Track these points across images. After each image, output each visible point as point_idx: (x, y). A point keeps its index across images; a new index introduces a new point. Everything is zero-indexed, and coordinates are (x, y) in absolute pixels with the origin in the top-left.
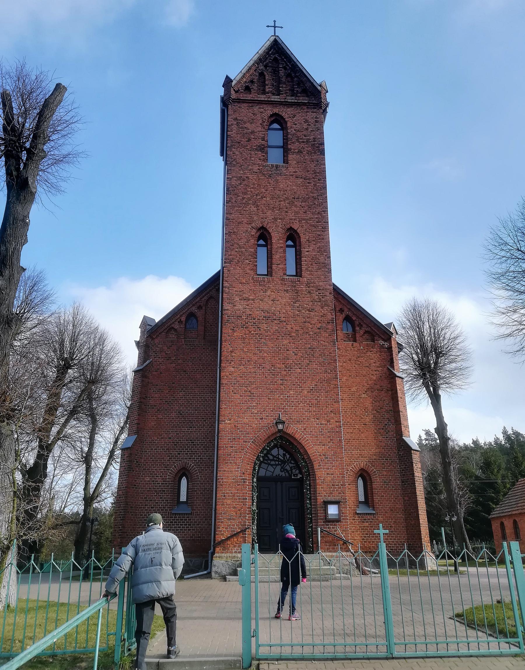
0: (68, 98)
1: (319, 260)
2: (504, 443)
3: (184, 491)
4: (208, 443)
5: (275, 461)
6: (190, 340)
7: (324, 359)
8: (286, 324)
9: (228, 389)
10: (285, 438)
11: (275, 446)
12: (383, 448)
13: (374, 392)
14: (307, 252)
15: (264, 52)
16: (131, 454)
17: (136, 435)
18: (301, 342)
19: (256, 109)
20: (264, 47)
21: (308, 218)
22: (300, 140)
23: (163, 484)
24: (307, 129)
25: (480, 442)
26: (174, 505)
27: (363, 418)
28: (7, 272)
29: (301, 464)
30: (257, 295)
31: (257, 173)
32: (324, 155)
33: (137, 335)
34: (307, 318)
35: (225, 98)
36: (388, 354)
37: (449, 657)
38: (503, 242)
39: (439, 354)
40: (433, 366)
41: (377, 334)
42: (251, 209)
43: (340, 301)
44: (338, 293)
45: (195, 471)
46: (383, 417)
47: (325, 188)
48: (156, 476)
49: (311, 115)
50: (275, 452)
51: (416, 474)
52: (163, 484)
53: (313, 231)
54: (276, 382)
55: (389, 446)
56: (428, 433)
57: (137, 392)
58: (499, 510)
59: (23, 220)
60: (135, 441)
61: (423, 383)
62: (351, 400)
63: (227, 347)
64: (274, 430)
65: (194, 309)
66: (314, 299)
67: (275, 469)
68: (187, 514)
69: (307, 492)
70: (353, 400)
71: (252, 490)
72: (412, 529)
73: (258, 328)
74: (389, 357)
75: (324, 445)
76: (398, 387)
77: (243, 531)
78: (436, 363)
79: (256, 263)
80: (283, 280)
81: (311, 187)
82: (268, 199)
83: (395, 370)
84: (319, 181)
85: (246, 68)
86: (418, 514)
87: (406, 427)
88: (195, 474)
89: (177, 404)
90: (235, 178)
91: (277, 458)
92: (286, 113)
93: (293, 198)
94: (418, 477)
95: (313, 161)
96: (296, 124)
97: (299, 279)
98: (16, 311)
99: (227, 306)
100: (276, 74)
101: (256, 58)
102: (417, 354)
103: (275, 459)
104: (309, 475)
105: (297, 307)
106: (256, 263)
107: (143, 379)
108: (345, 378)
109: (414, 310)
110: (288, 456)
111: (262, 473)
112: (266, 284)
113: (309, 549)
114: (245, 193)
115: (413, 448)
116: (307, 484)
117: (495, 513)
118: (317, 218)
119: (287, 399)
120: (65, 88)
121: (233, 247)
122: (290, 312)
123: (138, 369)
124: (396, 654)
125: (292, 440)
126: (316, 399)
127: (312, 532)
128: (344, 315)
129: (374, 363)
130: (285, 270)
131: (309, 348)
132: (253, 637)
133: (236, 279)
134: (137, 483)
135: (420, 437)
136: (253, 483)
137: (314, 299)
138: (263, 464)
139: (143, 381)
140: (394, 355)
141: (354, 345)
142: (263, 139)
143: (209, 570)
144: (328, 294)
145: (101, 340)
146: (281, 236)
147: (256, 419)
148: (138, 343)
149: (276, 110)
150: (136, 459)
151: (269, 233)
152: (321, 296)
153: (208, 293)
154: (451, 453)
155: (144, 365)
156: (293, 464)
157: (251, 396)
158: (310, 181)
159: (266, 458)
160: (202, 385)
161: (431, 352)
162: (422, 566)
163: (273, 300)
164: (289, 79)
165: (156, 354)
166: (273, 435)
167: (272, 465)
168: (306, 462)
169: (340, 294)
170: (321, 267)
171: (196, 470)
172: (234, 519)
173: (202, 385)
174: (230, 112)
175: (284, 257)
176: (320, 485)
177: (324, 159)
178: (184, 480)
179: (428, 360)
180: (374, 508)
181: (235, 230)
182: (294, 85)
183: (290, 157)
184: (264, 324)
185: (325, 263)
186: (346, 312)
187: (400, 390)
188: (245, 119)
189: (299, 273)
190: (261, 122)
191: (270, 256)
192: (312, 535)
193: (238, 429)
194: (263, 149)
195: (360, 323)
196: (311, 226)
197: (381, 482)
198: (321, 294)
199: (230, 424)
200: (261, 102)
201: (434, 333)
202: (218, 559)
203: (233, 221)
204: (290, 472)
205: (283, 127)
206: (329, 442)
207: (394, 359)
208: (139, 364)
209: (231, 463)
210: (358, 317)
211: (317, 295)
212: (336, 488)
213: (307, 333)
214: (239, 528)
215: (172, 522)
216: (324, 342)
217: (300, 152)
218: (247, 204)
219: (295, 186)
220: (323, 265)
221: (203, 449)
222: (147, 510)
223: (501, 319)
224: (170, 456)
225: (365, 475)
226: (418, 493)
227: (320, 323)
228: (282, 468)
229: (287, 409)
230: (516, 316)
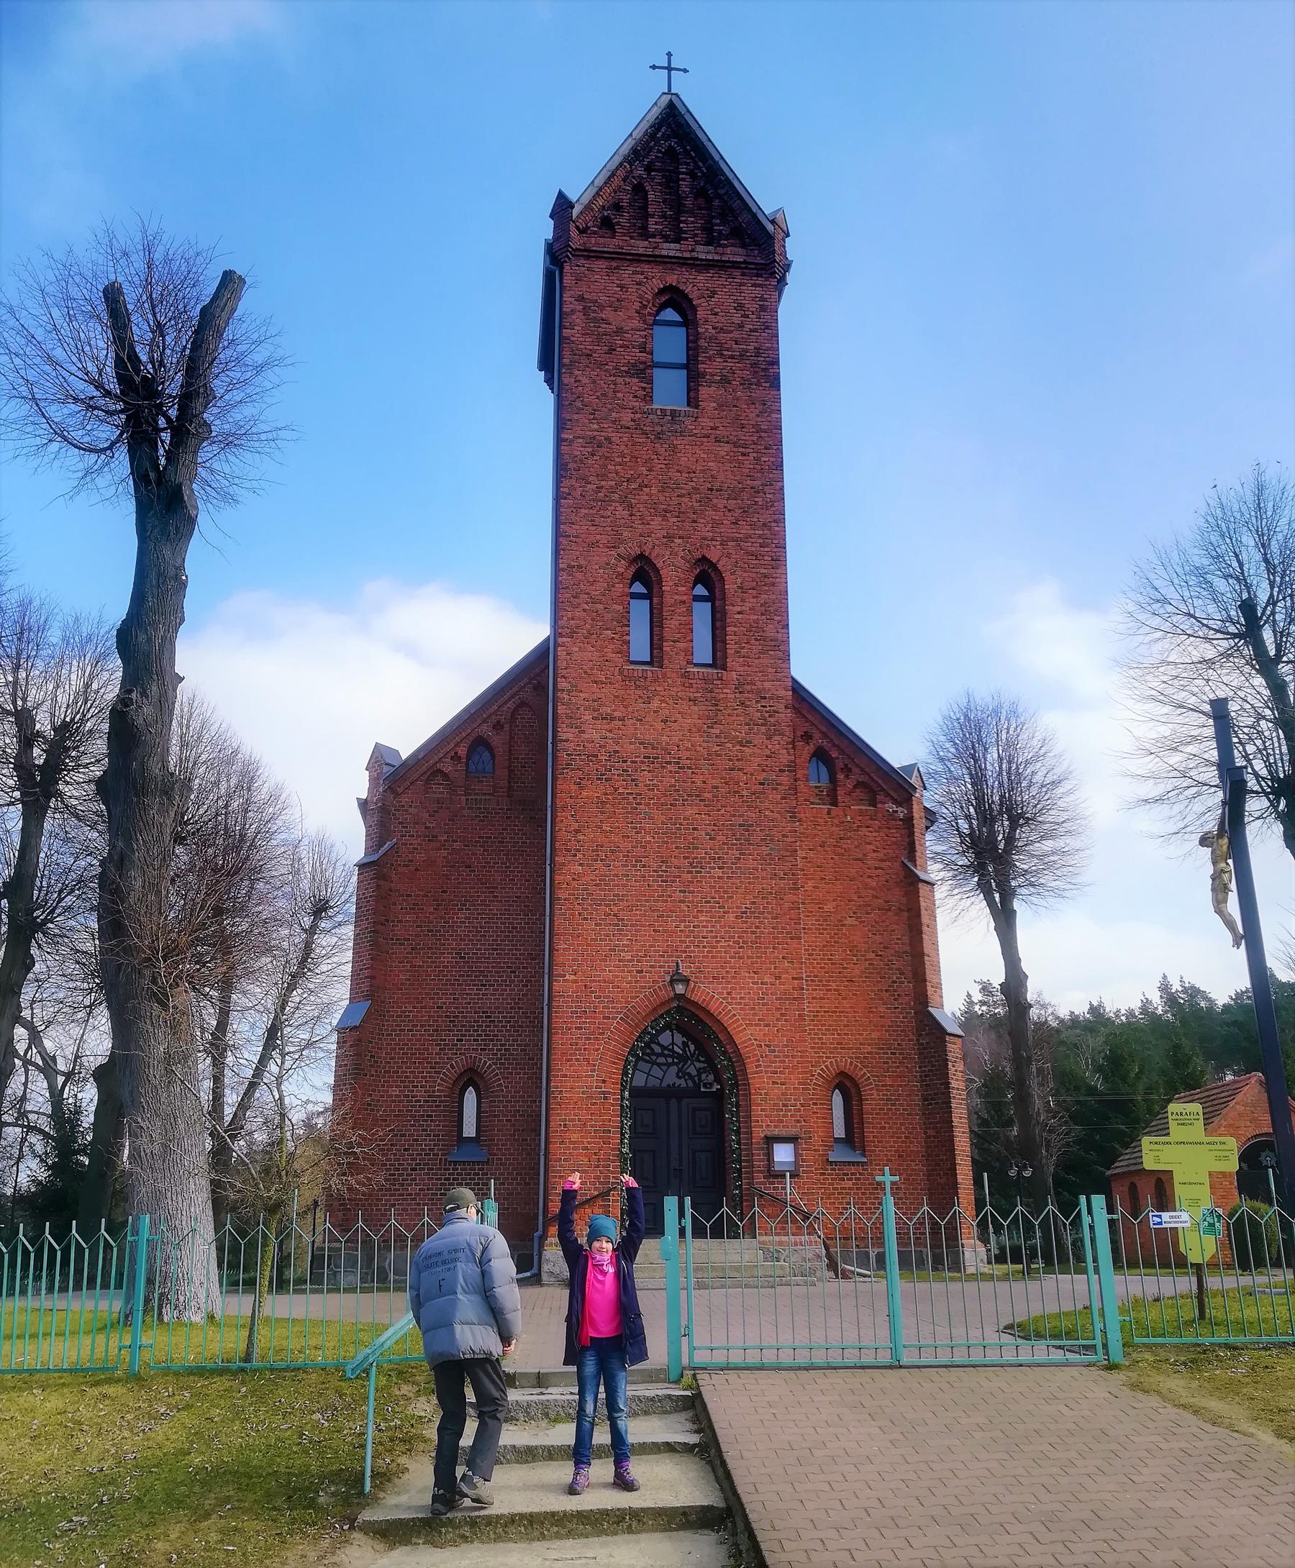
0: (248, 304)
1: (763, 631)
2: (1161, 1013)
3: (470, 1117)
4: (521, 1017)
5: (665, 1056)
6: (478, 798)
7: (771, 849)
8: (693, 773)
9: (569, 909)
10: (687, 1010)
11: (668, 1026)
12: (886, 1031)
13: (871, 913)
14: (739, 613)
15: (646, 133)
16: (360, 1040)
17: (368, 1000)
18: (723, 812)
19: (627, 273)
20: (643, 124)
21: (742, 536)
22: (726, 353)
23: (427, 1101)
24: (741, 326)
25: (1108, 1010)
26: (451, 1145)
27: (846, 968)
28: (154, 688)
29: (720, 1063)
30: (630, 709)
31: (629, 428)
32: (779, 390)
33: (361, 786)
34: (738, 760)
35: (556, 246)
36: (903, 832)
37: (985, 1366)
38: (1158, 596)
39: (1017, 818)
40: (1002, 846)
41: (883, 790)
42: (617, 513)
43: (805, 717)
44: (803, 701)
45: (494, 1076)
46: (888, 965)
47: (780, 466)
48: (413, 1086)
49: (751, 292)
50: (665, 1038)
51: (954, 1084)
52: (427, 1101)
53: (752, 566)
54: (670, 896)
55: (900, 1026)
56: (986, 988)
57: (368, 910)
58: (1129, 1159)
59: (177, 578)
60: (368, 1014)
61: (978, 884)
62: (823, 929)
63: (567, 822)
64: (665, 994)
67: (665, 1073)
68: (478, 1163)
69: (731, 1119)
70: (826, 929)
71: (621, 1115)
72: (942, 1194)
73: (633, 780)
74: (907, 840)
75: (768, 1025)
76: (922, 904)
77: (604, 1195)
78: (1010, 839)
79: (626, 638)
80: (686, 675)
81: (748, 464)
83: (918, 867)
84: (765, 451)
85: (606, 174)
86: (955, 1164)
87: (937, 987)
88: (495, 1082)
89: (452, 936)
90: (581, 440)
91: (669, 1050)
92: (694, 284)
93: (709, 489)
94: (958, 1089)
95: (753, 404)
96: (716, 314)
97: (720, 675)
98: (65, 717)
99: (566, 733)
100: (672, 188)
101: (626, 149)
102: (968, 817)
103: (666, 1052)
104: (736, 1085)
105: (717, 737)
106: (626, 638)
107: (380, 882)
108: (811, 883)
109: (966, 716)
110: (692, 1047)
111: (640, 1080)
112: (648, 684)
113: (734, 1229)
114: (603, 477)
115: (949, 1030)
116: (731, 1104)
117: (1121, 1164)
118: (760, 536)
119: (693, 932)
120: (242, 281)
121: (577, 600)
122: (700, 746)
123: (366, 860)
124: (904, 1361)
125: (702, 1015)
126: (753, 933)
127: (741, 1197)
128: (810, 748)
129: (874, 851)
130: (689, 652)
131: (740, 825)
132: (685, 1335)
133: (585, 672)
135: (969, 996)
136: (622, 1101)
137: (751, 720)
138: (641, 1062)
139: (378, 886)
140: (916, 834)
141: (833, 814)
142: (643, 348)
143: (535, 1270)
144: (781, 707)
145: (248, 780)
146: (682, 575)
147: (628, 972)
148: (363, 805)
149: (672, 279)
150: (369, 1052)
151: (657, 570)
152: (767, 712)
153: (516, 694)
154: (1034, 1038)
155: (381, 852)
156: (703, 1062)
158: (748, 450)
159: (648, 1051)
160: (507, 897)
161: (1001, 813)
162: (957, 1265)
163: (665, 721)
164: (701, 201)
165: (404, 827)
166: (662, 1004)
167: (659, 1065)
168: (730, 1060)
169: (804, 699)
170: (769, 648)
171: (497, 1074)
173: (507, 897)
174: (568, 280)
175: (689, 624)
176: (758, 1105)
177: (777, 399)
179: (992, 833)
180: (864, 1151)
181: (583, 562)
182: (714, 217)
183: (704, 392)
184: (646, 773)
185: (776, 640)
186: (818, 740)
187: (926, 910)
189: (719, 660)
191: (657, 622)
192: (742, 1203)
194: (643, 371)
195: (846, 765)
196: (748, 553)
197: (880, 1099)
198: (768, 709)
199: (575, 981)
200: (637, 259)
201: (1009, 773)
202: (554, 1247)
203: (577, 540)
204: (696, 1078)
205: (688, 320)
206: (777, 1020)
207: (917, 842)
208: (369, 850)
209: (578, 1060)
210: (842, 751)
214: (596, 1189)
215: (449, 1179)
216: (772, 812)
217: (725, 381)
218: (606, 501)
219: (713, 461)
220: (773, 643)
221: (509, 1031)
222: (395, 1155)
223: (1150, 764)
224: (440, 1045)
225: (849, 1085)
226: (956, 1121)
227: (764, 771)
228: (680, 1070)
230: (1175, 759)
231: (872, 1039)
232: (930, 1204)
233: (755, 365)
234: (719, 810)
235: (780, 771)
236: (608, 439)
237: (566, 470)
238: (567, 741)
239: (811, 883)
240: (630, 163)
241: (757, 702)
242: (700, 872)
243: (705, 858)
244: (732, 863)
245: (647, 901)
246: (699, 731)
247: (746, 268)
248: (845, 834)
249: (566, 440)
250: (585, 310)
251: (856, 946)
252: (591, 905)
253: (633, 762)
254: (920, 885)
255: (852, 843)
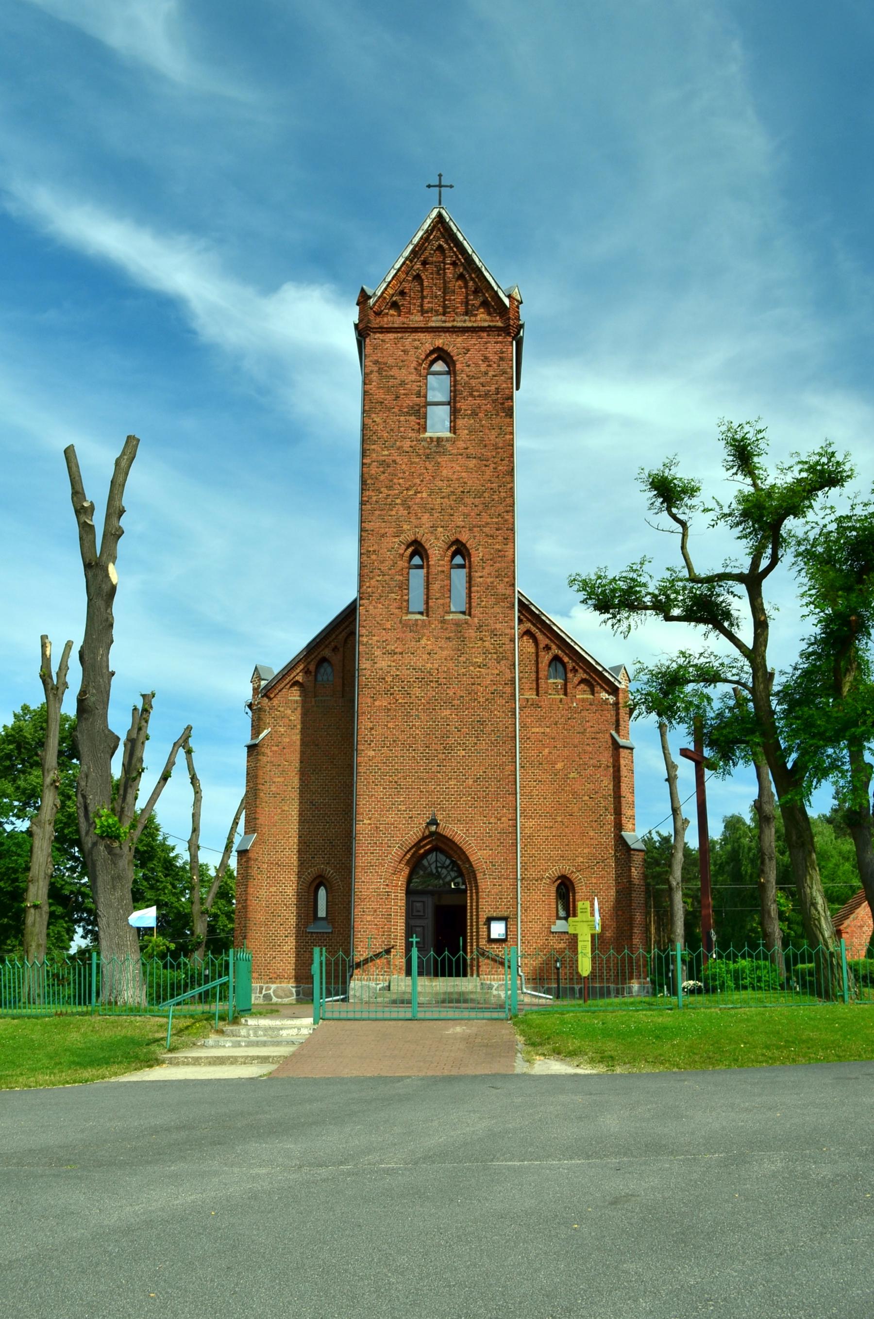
18: (467, 713)
19: (409, 340)
24: (486, 373)
31: (408, 452)
34: (477, 678)
35: (361, 326)
41: (599, 684)
54: (431, 769)
65: (327, 653)
66: (487, 650)
68: (326, 933)
73: (408, 694)
80: (444, 621)
81: (489, 472)
82: (424, 495)
92: (453, 344)
129: (592, 727)
131: (478, 721)
133: (378, 623)
134: (260, 895)
142: (418, 395)
149: (439, 342)
157: (397, 788)
163: (429, 654)
171: (337, 879)
172: (376, 938)
178: (322, 890)
183: (460, 422)
188: (391, 361)
190: (414, 364)
193: (380, 831)
194: (419, 412)
197: (587, 892)
199: (370, 824)
205: (452, 371)
206: (498, 846)
207: (621, 719)
209: (371, 872)
211: (492, 644)
212: (503, 902)
213: (475, 699)
217: (474, 414)
218: (392, 505)
227: (494, 684)
229: (445, 804)
231: (584, 854)
232: (434, 951)
233: (494, 401)
234: (463, 712)
235: (505, 684)
236: (394, 461)
237: (366, 485)
238: (365, 669)
239: (547, 750)
240: (411, 261)
241: (491, 638)
242: (450, 753)
243: (454, 744)
244: (472, 746)
245: (416, 772)
246: (452, 659)
247: (491, 331)
248: (572, 716)
249: (366, 464)
250: (380, 371)
251: (577, 792)
252: (380, 776)
253: (408, 682)
254: (621, 750)
255: (576, 722)
